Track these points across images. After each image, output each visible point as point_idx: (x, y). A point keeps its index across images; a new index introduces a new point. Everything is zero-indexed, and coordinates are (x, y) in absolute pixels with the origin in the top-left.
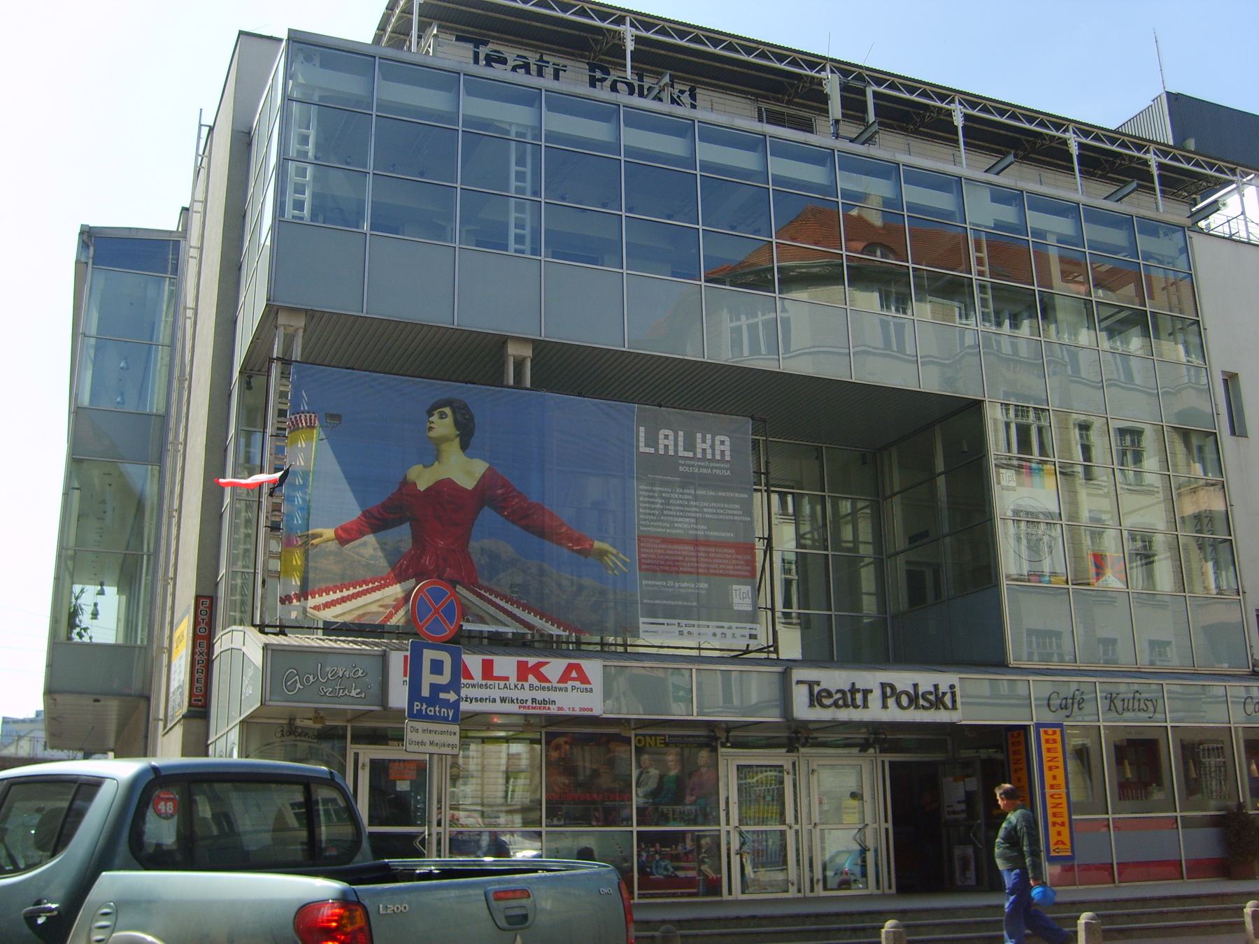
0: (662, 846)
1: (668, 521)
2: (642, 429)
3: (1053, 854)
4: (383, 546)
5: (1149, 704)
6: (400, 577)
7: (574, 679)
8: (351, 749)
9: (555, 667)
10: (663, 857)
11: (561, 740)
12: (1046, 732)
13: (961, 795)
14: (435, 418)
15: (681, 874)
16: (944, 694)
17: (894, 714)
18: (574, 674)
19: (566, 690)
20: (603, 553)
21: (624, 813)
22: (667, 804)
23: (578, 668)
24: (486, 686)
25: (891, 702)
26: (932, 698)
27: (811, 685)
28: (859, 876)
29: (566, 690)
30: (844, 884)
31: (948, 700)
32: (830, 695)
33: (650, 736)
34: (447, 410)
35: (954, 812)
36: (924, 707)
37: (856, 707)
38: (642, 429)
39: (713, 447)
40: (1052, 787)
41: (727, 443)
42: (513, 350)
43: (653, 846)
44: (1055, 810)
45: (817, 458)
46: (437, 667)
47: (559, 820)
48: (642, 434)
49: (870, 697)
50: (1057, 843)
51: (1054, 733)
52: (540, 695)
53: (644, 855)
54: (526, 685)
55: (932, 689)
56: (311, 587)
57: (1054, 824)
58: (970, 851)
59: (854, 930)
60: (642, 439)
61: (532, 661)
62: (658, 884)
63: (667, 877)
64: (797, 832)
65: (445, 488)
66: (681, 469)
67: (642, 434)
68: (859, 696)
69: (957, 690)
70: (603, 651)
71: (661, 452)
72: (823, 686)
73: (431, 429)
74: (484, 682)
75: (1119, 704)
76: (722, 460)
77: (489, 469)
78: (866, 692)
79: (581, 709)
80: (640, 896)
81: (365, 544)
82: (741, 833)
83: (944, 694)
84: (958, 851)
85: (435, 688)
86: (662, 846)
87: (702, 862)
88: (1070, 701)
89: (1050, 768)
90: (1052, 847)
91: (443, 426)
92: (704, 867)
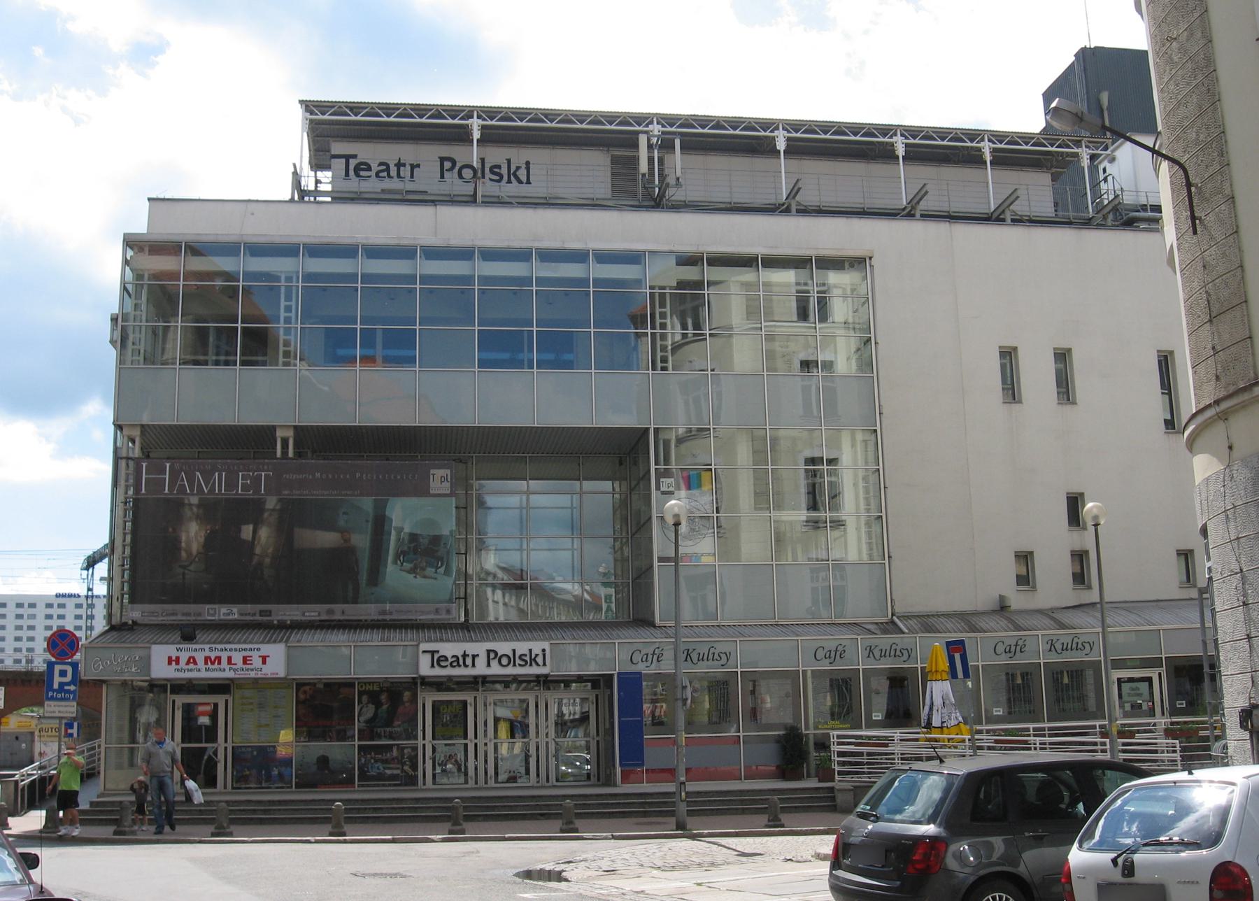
8: (170, 697)
10: (376, 761)
11: (307, 688)
15: (388, 772)
21: (349, 733)
25: (494, 663)
26: (528, 658)
27: (433, 653)
30: (512, 779)
31: (540, 660)
37: (466, 666)
42: (280, 434)
46: (63, 674)
49: (477, 660)
68: (469, 661)
78: (474, 657)
82: (557, 743)
85: (62, 685)
87: (403, 764)
92: (406, 768)
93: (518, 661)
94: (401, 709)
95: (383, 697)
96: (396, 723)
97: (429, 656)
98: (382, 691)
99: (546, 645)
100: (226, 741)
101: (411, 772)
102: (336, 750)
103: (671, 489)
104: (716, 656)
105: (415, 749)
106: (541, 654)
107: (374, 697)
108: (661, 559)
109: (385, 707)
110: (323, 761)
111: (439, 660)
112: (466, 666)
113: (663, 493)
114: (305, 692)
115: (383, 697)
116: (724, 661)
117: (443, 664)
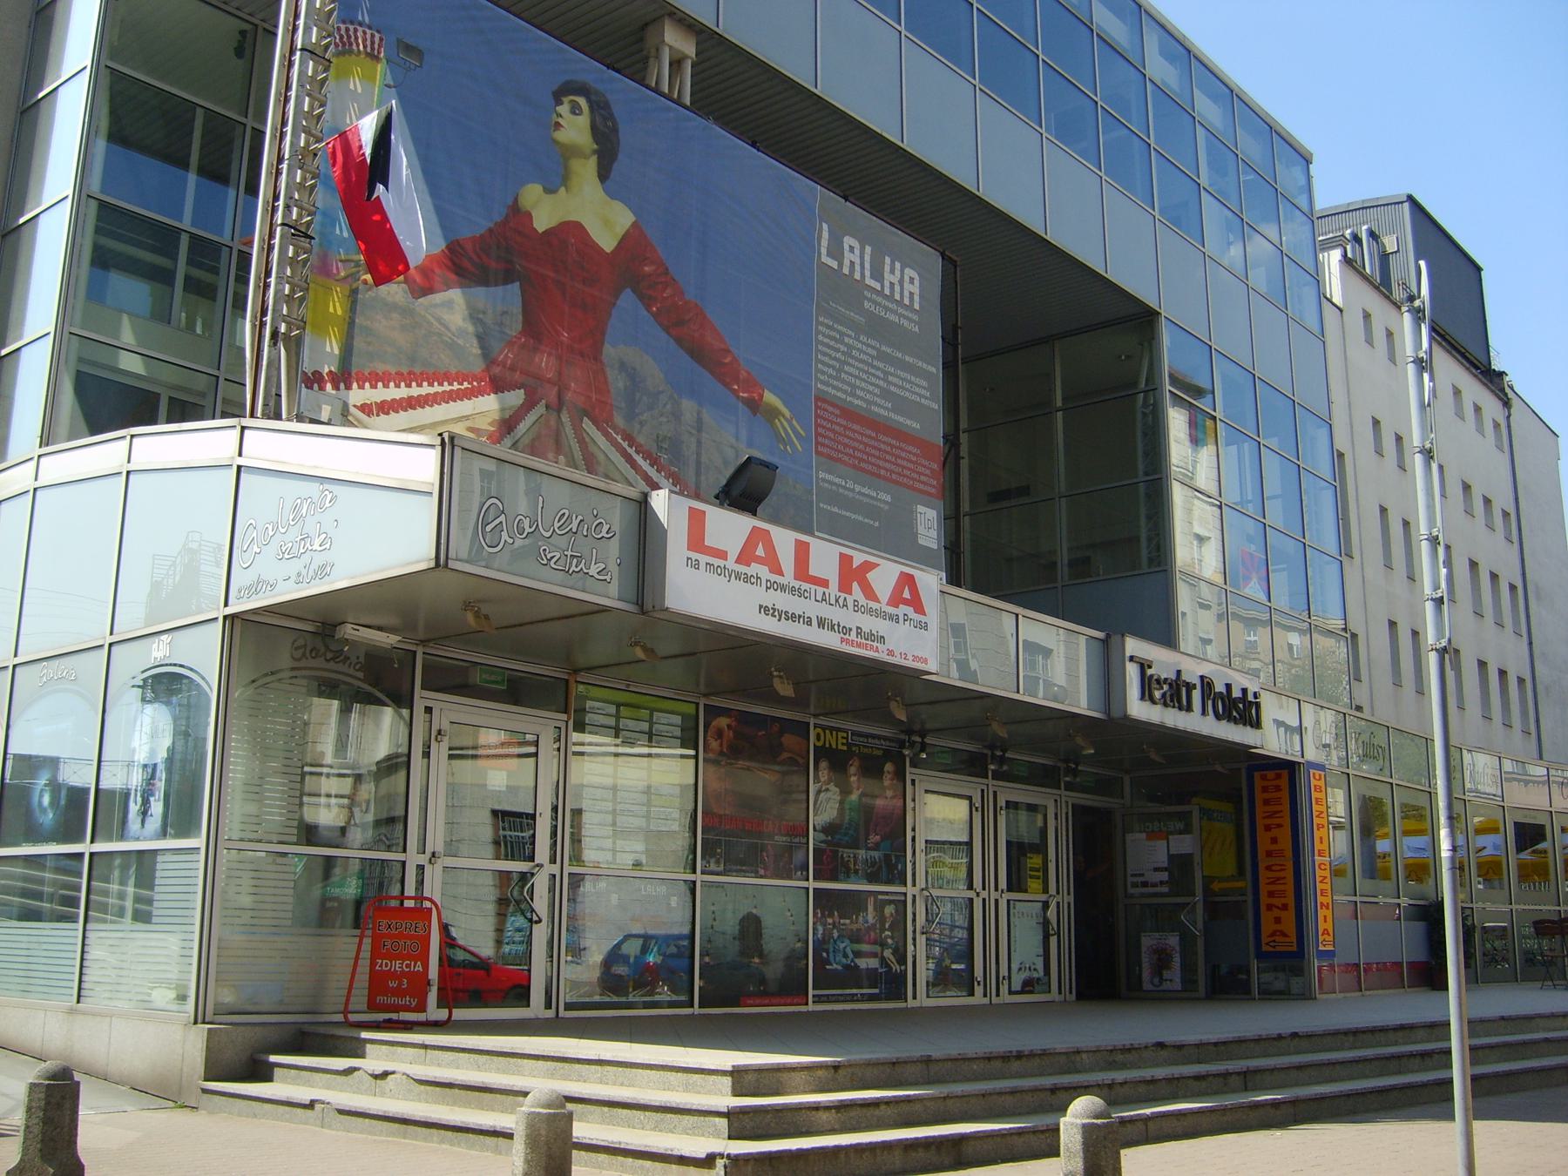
1: (849, 384)
2: (825, 226)
3: (1265, 948)
4: (474, 316)
6: (497, 386)
11: (723, 722)
12: (1264, 778)
13: (1162, 859)
14: (564, 109)
20: (773, 413)
24: (802, 594)
33: (832, 729)
34: (582, 101)
35: (1145, 884)
38: (825, 226)
39: (901, 282)
40: (1269, 854)
41: (917, 282)
44: (1272, 888)
48: (825, 235)
50: (1272, 935)
51: (1279, 776)
56: (357, 364)
57: (1270, 907)
58: (1173, 940)
60: (824, 243)
63: (847, 967)
65: (571, 232)
66: (867, 304)
67: (825, 235)
71: (846, 271)
73: (558, 126)
74: (797, 584)
76: (910, 308)
77: (635, 225)
79: (915, 658)
80: (818, 999)
81: (449, 304)
84: (1148, 941)
89: (1268, 828)
90: (1264, 939)
91: (575, 128)
92: (888, 953)
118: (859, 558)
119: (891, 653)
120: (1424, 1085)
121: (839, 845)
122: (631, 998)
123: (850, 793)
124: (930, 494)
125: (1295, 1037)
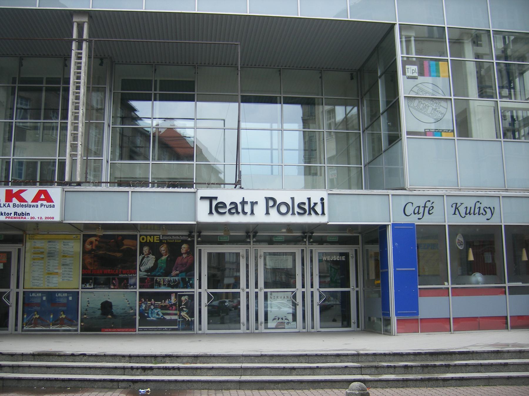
0: (155, 301)
5: (488, 210)
7: (43, 200)
9: (30, 193)
10: (156, 307)
11: (93, 239)
15: (168, 317)
16: (315, 204)
17: (274, 218)
18: (43, 197)
19: (37, 206)
21: (131, 281)
22: (159, 276)
23: (46, 193)
25: (273, 211)
26: (306, 207)
27: (211, 199)
28: (290, 317)
29: (37, 206)
31: (318, 209)
32: (224, 205)
33: (150, 236)
36: (299, 213)
37: (245, 213)
43: (150, 300)
45: (320, 78)
47: (90, 285)
49: (256, 208)
52: (19, 210)
53: (144, 306)
54: (11, 204)
55: (307, 202)
59: (144, 369)
61: (15, 189)
62: (152, 323)
63: (158, 318)
64: (248, 293)
69: (326, 201)
70: (62, 183)
72: (219, 200)
75: (462, 210)
78: (253, 204)
79: (46, 218)
83: (315, 204)
86: (155, 301)
87: (181, 310)
88: (421, 210)
92: (183, 314)
93: (297, 209)
94: (179, 260)
95: (163, 249)
96: (174, 273)
97: (207, 203)
98: (161, 242)
99: (324, 194)
100: (18, 287)
101: (188, 318)
102: (122, 298)
103: (416, 75)
104: (482, 211)
105: (191, 297)
106: (319, 202)
107: (154, 248)
108: (408, 133)
109: (164, 258)
110: (107, 307)
111: (218, 207)
112: (245, 213)
113: (409, 78)
114: (91, 243)
115: (163, 249)
116: (489, 215)
117: (221, 210)
118: (15, 189)
119: (33, 218)
120: (95, 381)
121: (155, 276)
122: (51, 328)
123: (162, 255)
124: (514, 92)
125: (114, 357)
